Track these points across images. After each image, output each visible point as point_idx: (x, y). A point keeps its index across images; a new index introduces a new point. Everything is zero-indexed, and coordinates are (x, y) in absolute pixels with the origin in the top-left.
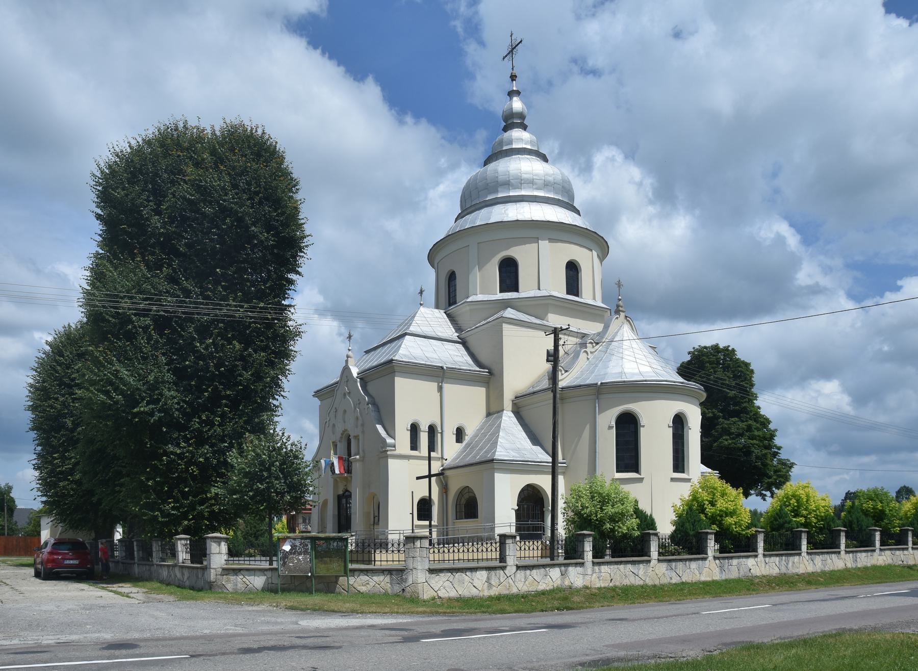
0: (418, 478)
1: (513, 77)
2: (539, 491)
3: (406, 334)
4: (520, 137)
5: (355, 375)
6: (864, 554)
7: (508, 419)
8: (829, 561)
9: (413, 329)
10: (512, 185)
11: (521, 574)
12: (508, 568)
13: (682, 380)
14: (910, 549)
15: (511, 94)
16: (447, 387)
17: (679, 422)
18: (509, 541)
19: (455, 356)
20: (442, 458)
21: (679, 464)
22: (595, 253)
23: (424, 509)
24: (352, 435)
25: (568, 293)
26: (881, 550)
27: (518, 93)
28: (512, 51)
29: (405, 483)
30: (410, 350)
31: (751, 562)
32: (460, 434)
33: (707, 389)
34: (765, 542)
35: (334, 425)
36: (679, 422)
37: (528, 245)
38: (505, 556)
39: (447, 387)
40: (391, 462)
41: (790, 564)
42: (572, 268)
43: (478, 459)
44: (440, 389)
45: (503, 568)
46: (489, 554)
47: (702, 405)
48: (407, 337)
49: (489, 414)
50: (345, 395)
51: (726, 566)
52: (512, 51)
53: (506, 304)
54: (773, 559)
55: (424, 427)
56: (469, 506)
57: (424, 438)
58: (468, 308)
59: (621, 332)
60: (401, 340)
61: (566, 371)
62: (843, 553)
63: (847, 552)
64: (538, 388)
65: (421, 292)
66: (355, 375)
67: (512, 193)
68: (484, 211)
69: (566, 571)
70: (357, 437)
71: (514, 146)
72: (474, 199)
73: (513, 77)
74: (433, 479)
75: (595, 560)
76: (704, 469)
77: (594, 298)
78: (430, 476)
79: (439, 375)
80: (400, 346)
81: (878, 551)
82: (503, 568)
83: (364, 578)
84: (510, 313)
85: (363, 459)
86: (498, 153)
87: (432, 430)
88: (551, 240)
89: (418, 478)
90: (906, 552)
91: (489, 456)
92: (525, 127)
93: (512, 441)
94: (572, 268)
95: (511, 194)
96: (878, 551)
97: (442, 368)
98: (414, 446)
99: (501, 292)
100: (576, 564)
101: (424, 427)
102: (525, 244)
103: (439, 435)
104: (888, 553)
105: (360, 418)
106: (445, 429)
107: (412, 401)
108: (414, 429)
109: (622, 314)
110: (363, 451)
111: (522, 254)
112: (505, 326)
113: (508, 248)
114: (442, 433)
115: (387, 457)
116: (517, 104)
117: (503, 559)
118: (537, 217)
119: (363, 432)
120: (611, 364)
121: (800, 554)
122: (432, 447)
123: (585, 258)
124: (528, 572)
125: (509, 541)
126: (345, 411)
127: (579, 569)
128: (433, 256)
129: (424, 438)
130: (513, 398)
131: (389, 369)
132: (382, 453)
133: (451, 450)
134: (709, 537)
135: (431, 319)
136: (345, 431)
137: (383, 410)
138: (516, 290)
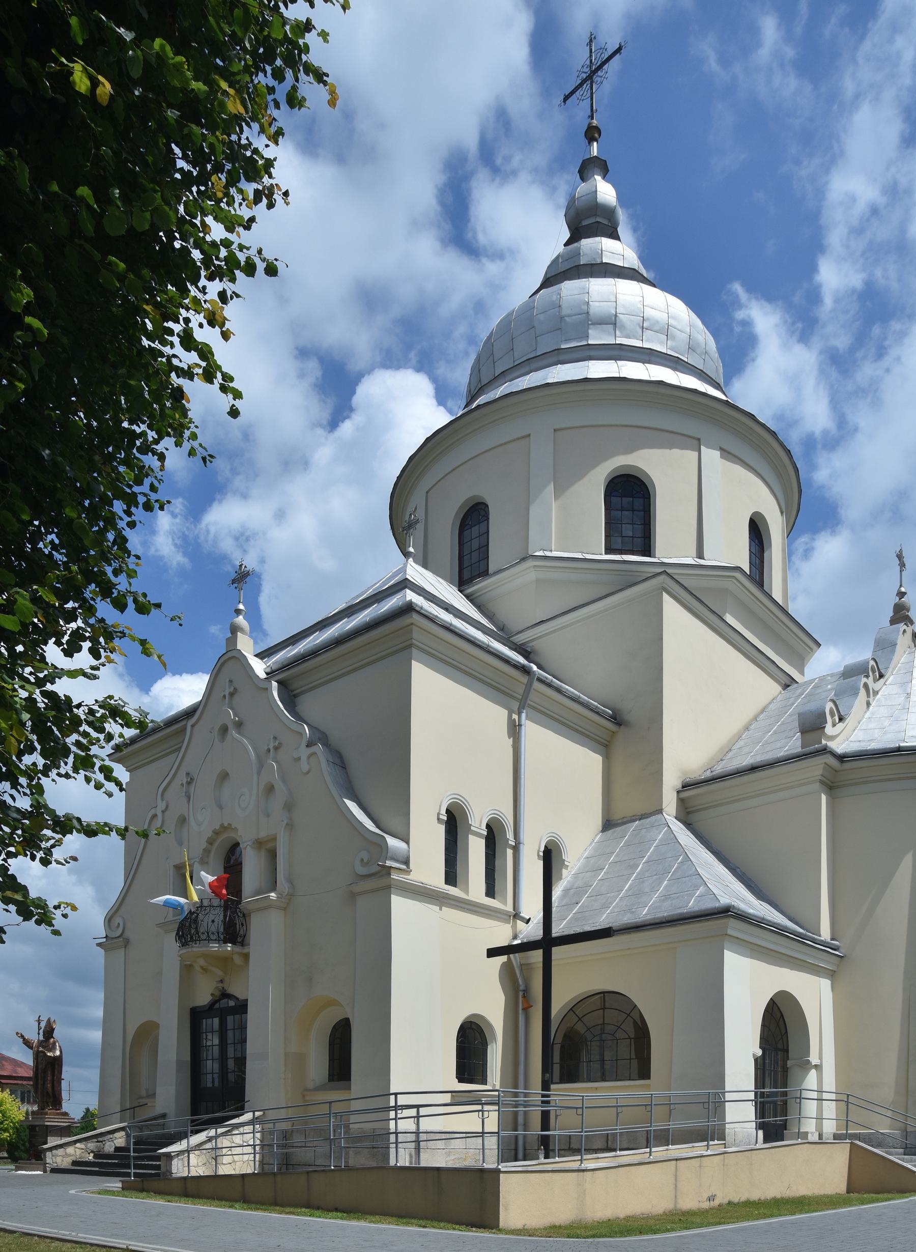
1: (592, 133)
10: (623, 327)
20: (516, 916)
23: (471, 1042)
24: (246, 837)
28: (590, 78)
29: (440, 970)
37: (676, 452)
44: (514, 730)
49: (608, 825)
50: (224, 730)
52: (590, 78)
57: (476, 849)
58: (532, 576)
83: (60, 1152)
85: (286, 905)
88: (726, 454)
99: (606, 553)
101: (478, 821)
102: (671, 447)
103: (510, 852)
105: (279, 786)
106: (525, 836)
108: (454, 823)
110: (290, 880)
111: (668, 471)
113: (630, 451)
114: (516, 849)
115: (387, 890)
126: (224, 776)
129: (476, 849)
130: (679, 786)
132: (375, 877)
136: (224, 828)
137: (375, 762)
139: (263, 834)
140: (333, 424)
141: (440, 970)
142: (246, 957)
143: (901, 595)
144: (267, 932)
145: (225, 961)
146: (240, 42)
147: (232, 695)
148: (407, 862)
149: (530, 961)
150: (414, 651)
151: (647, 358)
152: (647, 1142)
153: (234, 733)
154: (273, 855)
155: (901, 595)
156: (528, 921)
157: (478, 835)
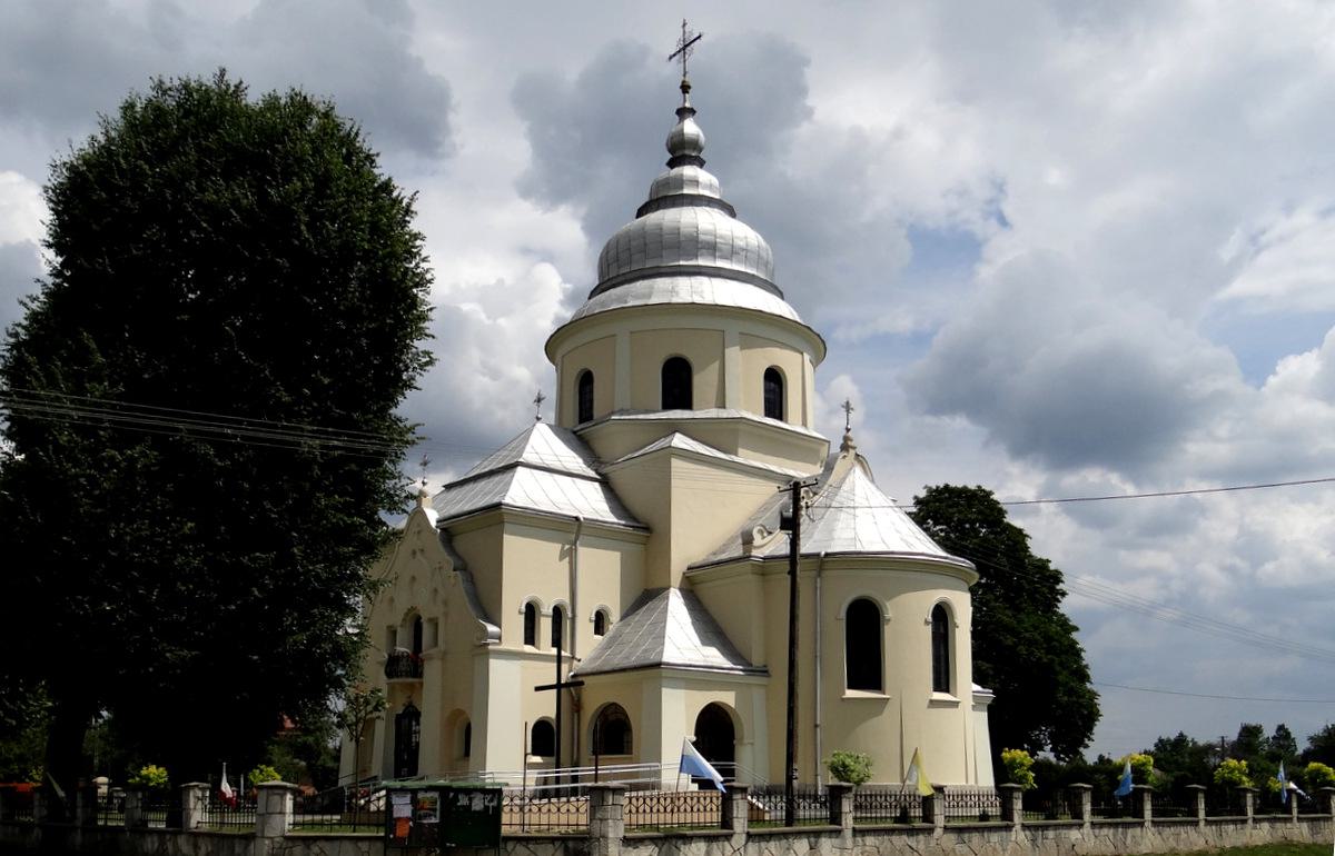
0: (538, 689)
2: (727, 714)
3: (517, 464)
4: (701, 178)
5: (433, 524)
6: (1232, 827)
7: (676, 604)
8: (1184, 836)
9: (528, 456)
11: (752, 848)
12: (735, 838)
13: (942, 553)
14: (1087, 828)
15: (683, 113)
16: (584, 553)
17: (941, 615)
18: (737, 796)
19: (589, 501)
20: (573, 658)
21: (943, 680)
22: (807, 357)
25: (768, 414)
26: (1255, 820)
27: (692, 111)
29: (515, 695)
30: (523, 491)
31: (1074, 834)
32: (600, 622)
33: (981, 569)
34: (1205, 803)
35: (392, 600)
36: (941, 615)
38: (732, 819)
39: (584, 553)
40: (494, 664)
41: (1129, 841)
42: (774, 378)
43: (633, 661)
45: (930, 831)
46: (641, 817)
47: (972, 591)
48: (519, 469)
50: (414, 553)
51: (1040, 840)
53: (673, 427)
54: (1105, 831)
55: (547, 609)
56: (616, 734)
57: (545, 627)
59: (850, 478)
60: (506, 476)
61: (770, 533)
62: (1202, 824)
63: (1208, 823)
64: (724, 556)
65: (539, 400)
66: (433, 524)
67: (701, 262)
68: (641, 285)
69: (816, 842)
70: (434, 622)
71: (686, 191)
72: (626, 261)
73: (685, 88)
74: (563, 690)
75: (1257, 816)
76: (977, 688)
77: (804, 424)
78: (558, 686)
79: (568, 530)
80: (509, 483)
81: (1250, 821)
82: (728, 837)
84: (679, 441)
86: (665, 197)
87: (558, 613)
89: (538, 689)
90: (1289, 825)
91: (653, 658)
92: (701, 164)
93: (681, 640)
94: (774, 378)
95: (682, 263)
96: (1250, 821)
97: (577, 519)
98: (530, 638)
100: (1234, 822)
104: (1266, 826)
107: (529, 572)
108: (531, 612)
109: (852, 452)
112: (676, 463)
116: (690, 128)
117: (727, 822)
118: (708, 299)
119: (446, 615)
120: (840, 525)
121: (1142, 825)
122: (557, 642)
123: (792, 363)
124: (763, 844)
125: (737, 796)
126: (413, 578)
127: (835, 841)
128: (552, 347)
129: (545, 627)
130: (685, 569)
131: (495, 517)
132: (481, 651)
133: (587, 646)
134: (1016, 794)
135: (545, 444)
136: (413, 609)
138: (688, 405)
139: (432, 616)
140: (637, 217)
141: (515, 695)
142: (421, 684)
143: (848, 430)
144: (432, 672)
145: (412, 685)
146: (369, 242)
147: (419, 532)
148: (500, 638)
149: (569, 690)
150: (506, 525)
151: (588, 405)
152: (645, 787)
153: (418, 554)
154: (437, 625)
155: (848, 430)
156: (579, 660)
157: (547, 616)
